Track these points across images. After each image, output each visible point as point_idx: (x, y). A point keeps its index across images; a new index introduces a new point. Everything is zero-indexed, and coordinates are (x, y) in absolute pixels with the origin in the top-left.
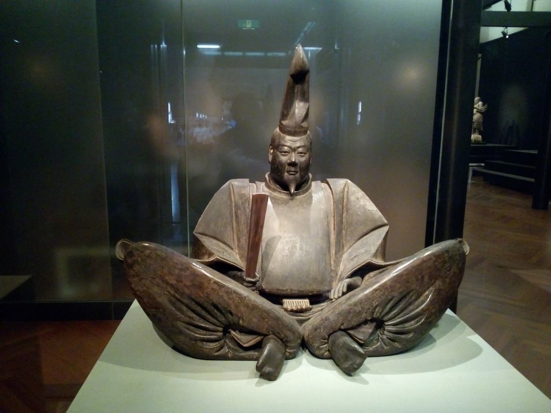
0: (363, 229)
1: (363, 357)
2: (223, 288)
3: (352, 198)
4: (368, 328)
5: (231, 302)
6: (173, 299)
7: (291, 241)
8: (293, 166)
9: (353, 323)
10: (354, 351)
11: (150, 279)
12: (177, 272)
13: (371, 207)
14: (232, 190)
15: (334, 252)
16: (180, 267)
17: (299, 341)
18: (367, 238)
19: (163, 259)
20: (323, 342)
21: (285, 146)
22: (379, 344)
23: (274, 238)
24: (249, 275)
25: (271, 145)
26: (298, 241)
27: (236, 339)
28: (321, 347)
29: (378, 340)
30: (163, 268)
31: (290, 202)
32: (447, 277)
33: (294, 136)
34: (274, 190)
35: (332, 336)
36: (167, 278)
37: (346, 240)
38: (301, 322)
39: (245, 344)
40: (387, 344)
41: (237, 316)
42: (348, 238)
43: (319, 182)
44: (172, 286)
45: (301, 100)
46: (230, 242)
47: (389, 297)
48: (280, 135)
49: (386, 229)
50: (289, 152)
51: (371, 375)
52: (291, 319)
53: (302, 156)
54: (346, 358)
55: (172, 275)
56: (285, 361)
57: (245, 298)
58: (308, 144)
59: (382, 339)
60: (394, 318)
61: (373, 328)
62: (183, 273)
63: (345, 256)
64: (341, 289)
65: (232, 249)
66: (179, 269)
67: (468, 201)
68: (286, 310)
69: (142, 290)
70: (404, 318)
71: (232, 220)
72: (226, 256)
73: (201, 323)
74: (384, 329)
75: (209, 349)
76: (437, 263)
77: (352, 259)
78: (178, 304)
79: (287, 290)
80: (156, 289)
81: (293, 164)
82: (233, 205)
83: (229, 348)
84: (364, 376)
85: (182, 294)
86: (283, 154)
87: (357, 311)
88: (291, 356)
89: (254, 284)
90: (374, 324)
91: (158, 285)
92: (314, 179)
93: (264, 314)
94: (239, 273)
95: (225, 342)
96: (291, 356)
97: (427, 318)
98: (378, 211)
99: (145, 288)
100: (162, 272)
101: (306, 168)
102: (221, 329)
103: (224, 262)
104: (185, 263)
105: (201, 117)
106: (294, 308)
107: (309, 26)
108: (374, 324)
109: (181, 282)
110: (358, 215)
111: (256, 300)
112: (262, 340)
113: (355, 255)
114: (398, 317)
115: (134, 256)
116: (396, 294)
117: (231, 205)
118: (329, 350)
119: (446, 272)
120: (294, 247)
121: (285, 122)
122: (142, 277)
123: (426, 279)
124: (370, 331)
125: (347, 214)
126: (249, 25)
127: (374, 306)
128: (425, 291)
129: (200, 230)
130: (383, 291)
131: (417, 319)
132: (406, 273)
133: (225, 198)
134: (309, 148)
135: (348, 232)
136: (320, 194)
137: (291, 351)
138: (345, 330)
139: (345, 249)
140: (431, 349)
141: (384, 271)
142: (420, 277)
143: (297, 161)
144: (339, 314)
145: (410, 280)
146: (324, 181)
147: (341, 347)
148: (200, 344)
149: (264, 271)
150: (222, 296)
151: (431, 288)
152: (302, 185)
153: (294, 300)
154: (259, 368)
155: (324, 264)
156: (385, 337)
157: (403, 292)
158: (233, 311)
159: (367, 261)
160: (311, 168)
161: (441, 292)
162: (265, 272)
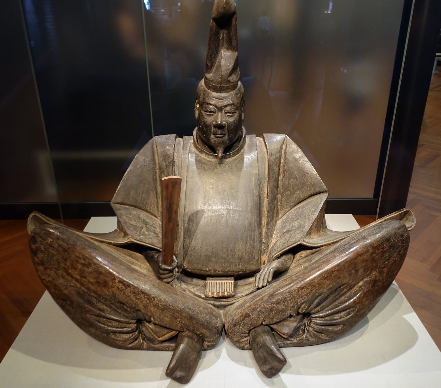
0: (298, 194)
2: (129, 288)
3: (290, 158)
4: (293, 322)
5: (139, 302)
11: (54, 269)
14: (155, 149)
19: (65, 251)
20: (242, 336)
21: (210, 104)
23: (197, 212)
24: (165, 263)
28: (242, 340)
31: (218, 166)
32: (385, 267)
34: (202, 152)
36: (70, 271)
37: (281, 205)
39: (159, 337)
42: (284, 203)
43: (254, 136)
44: (77, 280)
45: (228, 49)
50: (215, 113)
55: (75, 269)
56: (203, 352)
62: (86, 269)
63: (279, 223)
66: (81, 264)
67: (430, 93)
69: (47, 280)
73: (112, 315)
75: (121, 341)
77: (283, 234)
79: (210, 271)
80: (61, 281)
81: (220, 127)
82: (157, 167)
86: (208, 113)
87: (280, 309)
91: (63, 277)
98: (318, 175)
99: (50, 279)
100: (65, 265)
102: (134, 321)
104: (87, 257)
106: (215, 295)
109: (85, 277)
114: (326, 309)
117: (154, 168)
119: (384, 262)
122: (47, 266)
125: (283, 177)
127: (299, 304)
129: (119, 200)
130: (310, 289)
131: (348, 311)
136: (255, 152)
137: (209, 344)
139: (280, 216)
140: (361, 335)
141: (316, 252)
145: (342, 276)
146: (259, 135)
148: (113, 336)
149: (186, 249)
150: (129, 296)
155: (252, 242)
156: (311, 329)
159: (299, 243)
161: (377, 283)
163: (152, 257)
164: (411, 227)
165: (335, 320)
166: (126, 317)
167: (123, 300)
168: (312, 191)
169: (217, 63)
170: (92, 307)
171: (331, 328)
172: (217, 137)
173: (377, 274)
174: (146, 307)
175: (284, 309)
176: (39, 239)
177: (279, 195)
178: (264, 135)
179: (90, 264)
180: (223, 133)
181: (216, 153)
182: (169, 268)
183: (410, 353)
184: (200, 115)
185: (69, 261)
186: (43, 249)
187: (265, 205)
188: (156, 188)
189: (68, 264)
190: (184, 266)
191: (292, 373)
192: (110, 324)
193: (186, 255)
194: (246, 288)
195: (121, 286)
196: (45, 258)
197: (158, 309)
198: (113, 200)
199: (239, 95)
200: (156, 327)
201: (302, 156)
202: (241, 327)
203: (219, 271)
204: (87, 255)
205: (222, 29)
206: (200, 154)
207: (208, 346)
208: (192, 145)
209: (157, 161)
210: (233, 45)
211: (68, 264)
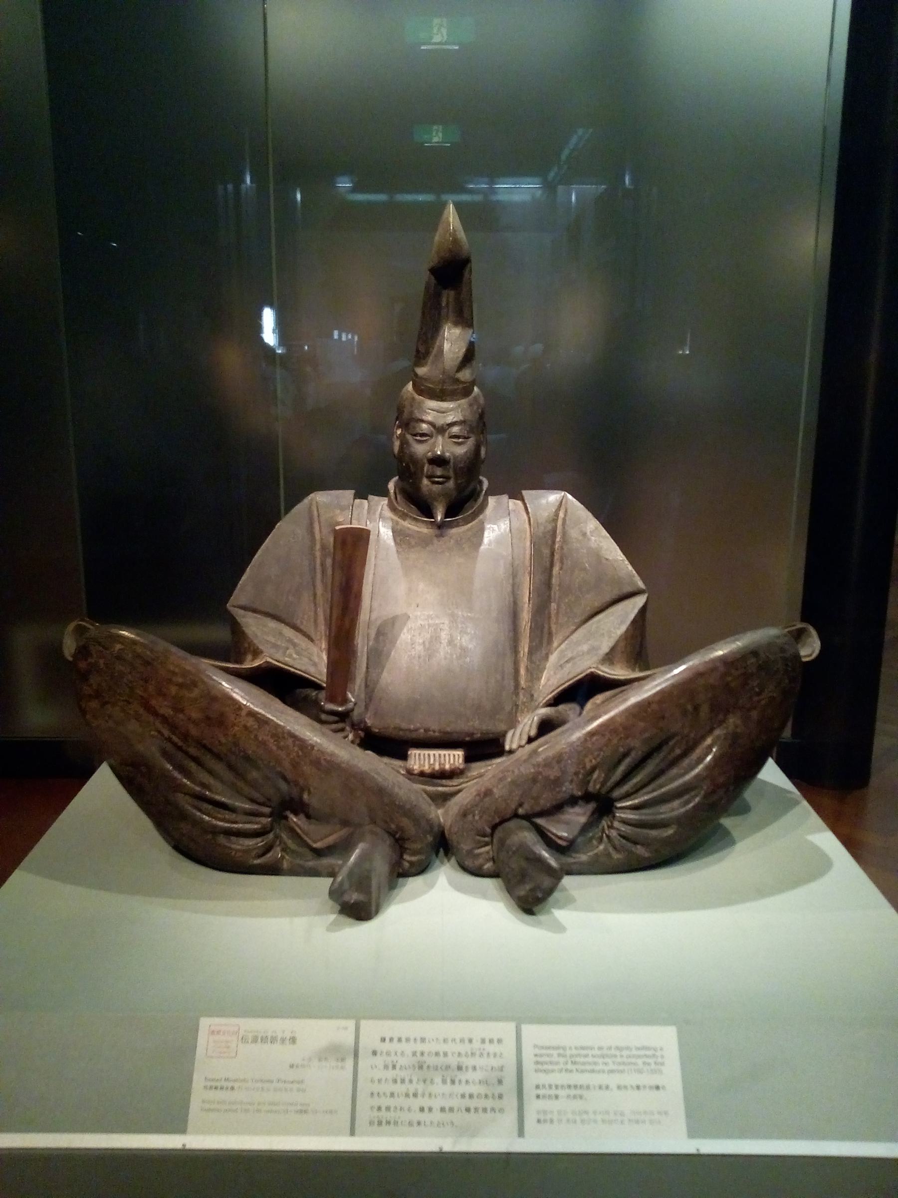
0: (593, 600)
1: (556, 875)
3: (574, 533)
4: (578, 814)
5: (282, 754)
6: (169, 747)
7: (429, 625)
8: (439, 465)
9: (542, 802)
10: (539, 861)
12: (173, 690)
13: (611, 550)
14: (315, 513)
15: (526, 650)
16: (180, 680)
17: (430, 838)
18: (599, 621)
19: (147, 663)
20: (479, 842)
21: (423, 421)
22: (601, 847)
24: (332, 699)
25: (397, 419)
26: (446, 627)
27: (299, 831)
29: (601, 840)
30: (146, 681)
31: (435, 541)
33: (442, 401)
34: (404, 516)
35: (500, 828)
36: (153, 702)
38: (442, 799)
39: (315, 842)
40: (618, 847)
41: (296, 784)
42: (563, 619)
43: (505, 498)
44: (165, 720)
45: (456, 324)
46: (310, 629)
47: (621, 750)
48: (413, 399)
49: (640, 601)
50: (431, 436)
51: (575, 914)
52: (413, 793)
53: (459, 444)
54: (523, 877)
57: (313, 747)
58: (472, 418)
59: (608, 837)
60: (633, 793)
61: (589, 813)
62: (185, 693)
63: (553, 658)
64: (527, 729)
65: (312, 640)
68: (410, 773)
70: (655, 794)
71: (313, 579)
72: (290, 656)
74: (614, 817)
76: (729, 679)
77: (561, 666)
78: (180, 755)
79: (416, 730)
81: (439, 461)
82: (318, 547)
83: (284, 850)
84: (560, 914)
85: (185, 737)
86: (418, 438)
87: (552, 777)
88: (413, 870)
89: (343, 717)
90: (592, 806)
91: (138, 718)
92: (492, 492)
93: (353, 781)
94: (314, 694)
95: (277, 837)
96: (413, 870)
97: (705, 797)
98: (627, 562)
99: (111, 724)
100: (145, 690)
101: (470, 469)
103: (282, 669)
104: (189, 672)
105: (344, 338)
106: (426, 768)
107: (578, 137)
108: (592, 806)
109: (182, 711)
110: (585, 569)
111: (336, 752)
112: (351, 835)
113: (570, 655)
114: (645, 790)
115: (91, 655)
116: (635, 743)
117: (312, 548)
118: (493, 860)
120: (435, 638)
121: (421, 371)
123: (705, 710)
124: (583, 820)
125: (561, 569)
126: (436, 137)
127: (588, 766)
128: (703, 738)
129: (243, 601)
130: (608, 736)
131: (686, 797)
132: (657, 698)
133: (301, 532)
134: (479, 425)
135: (563, 606)
137: (414, 859)
138: (528, 817)
139: (555, 644)
140: (720, 860)
142: (689, 707)
143: (447, 454)
144: (514, 783)
146: (516, 495)
147: (514, 853)
148: (222, 840)
149: (370, 687)
150: (264, 743)
151: (717, 732)
152: (463, 504)
153: (432, 752)
154: (334, 894)
155: (499, 677)
156: (614, 833)
157: (655, 741)
158: (289, 776)
160: (483, 468)
162: (373, 691)
163: (306, 698)
164: (811, 655)
165: (661, 813)
166: (253, 801)
167: (254, 752)
168: (616, 593)
169: (435, 349)
170: (188, 778)
171: (654, 833)
172: (434, 483)
173: (739, 722)
174: (295, 765)
175: (559, 778)
176: (94, 649)
177: (553, 604)
178: (524, 492)
179: (194, 684)
180: (446, 473)
181: (433, 518)
182: (340, 709)
183: (814, 886)
184: (404, 443)
185: (153, 682)
186: (102, 666)
187: (526, 616)
188: (314, 586)
189: (151, 688)
190: (366, 722)
191: (576, 909)
192: (219, 816)
193: (370, 700)
194: (488, 771)
195: (251, 722)
196: (104, 684)
197: (319, 769)
198: (233, 600)
199: (475, 407)
200: (310, 824)
201: (596, 528)
202: (477, 818)
203: (434, 732)
204: (188, 668)
205: (445, 289)
206: (401, 521)
207: (412, 863)
208: (386, 508)
209: (318, 537)
210: (465, 316)
211: (151, 688)
